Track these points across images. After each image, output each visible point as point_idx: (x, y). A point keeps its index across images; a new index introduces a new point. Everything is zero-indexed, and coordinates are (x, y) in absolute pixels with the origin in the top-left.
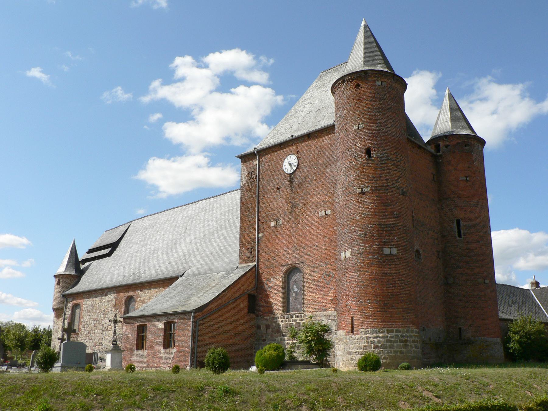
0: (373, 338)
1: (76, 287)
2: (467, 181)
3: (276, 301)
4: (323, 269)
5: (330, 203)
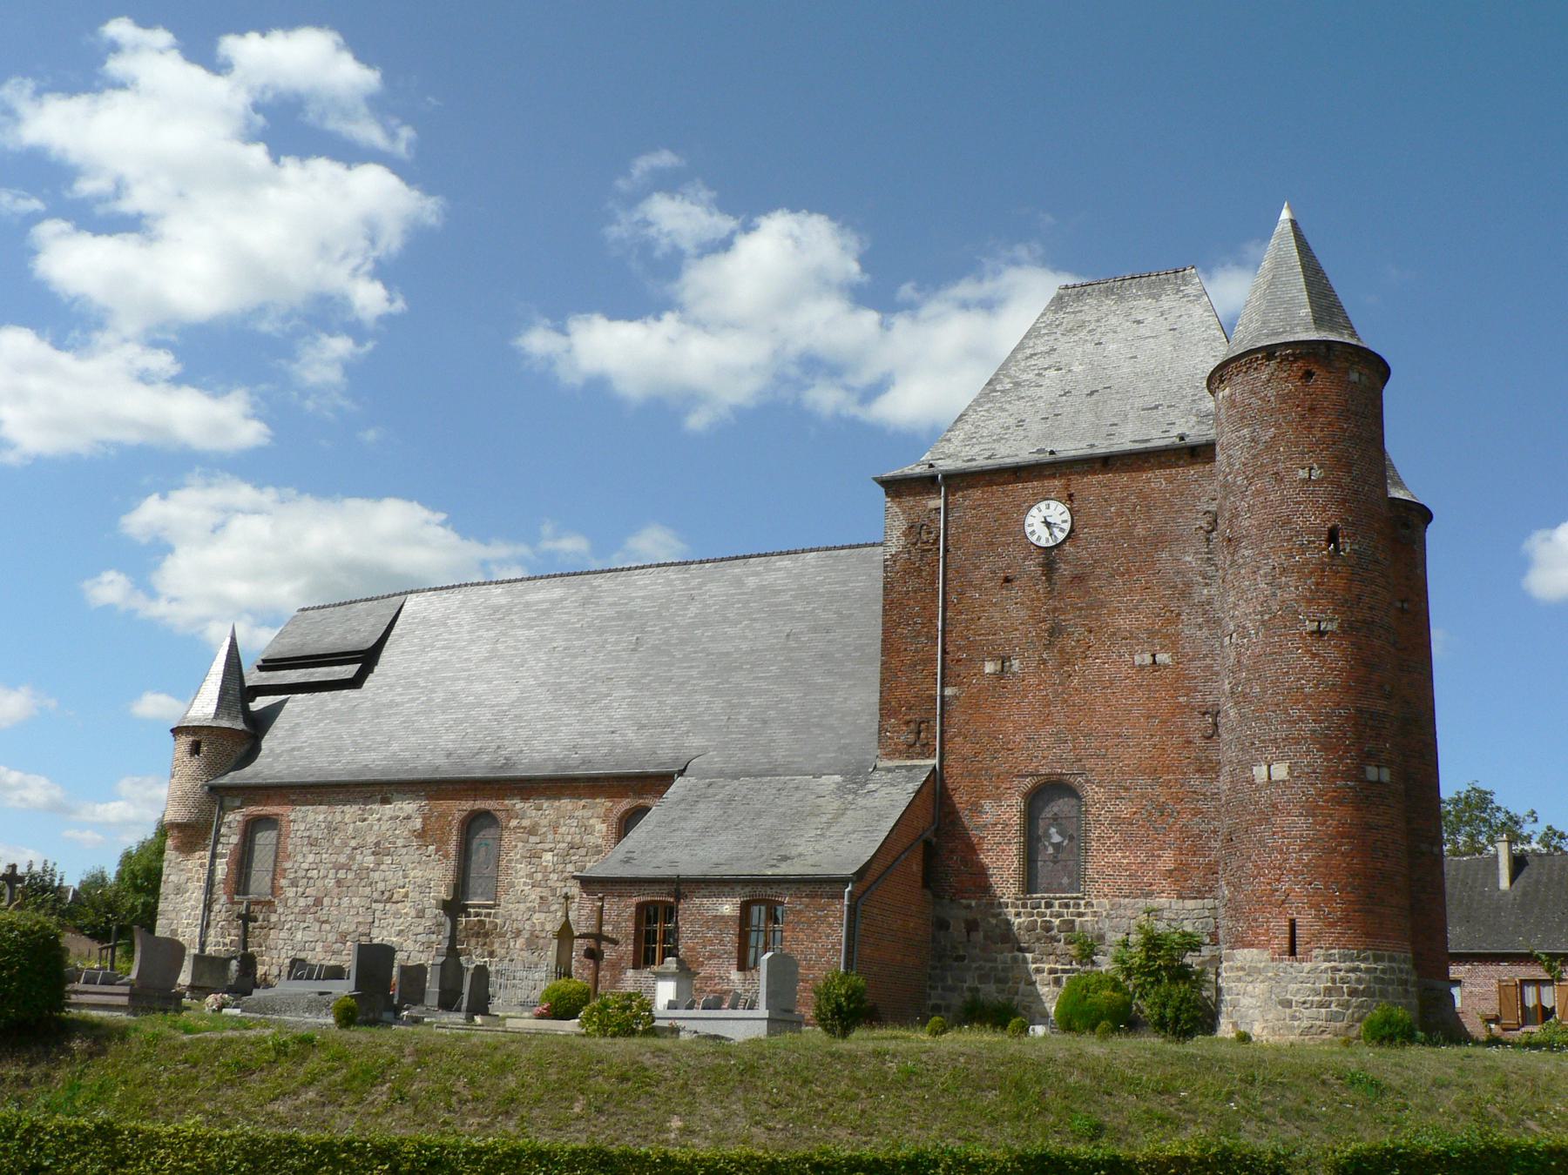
0: (1347, 971)
1: (248, 770)
2: (1402, 610)
3: (1002, 865)
4: (1143, 796)
5: (1167, 636)
